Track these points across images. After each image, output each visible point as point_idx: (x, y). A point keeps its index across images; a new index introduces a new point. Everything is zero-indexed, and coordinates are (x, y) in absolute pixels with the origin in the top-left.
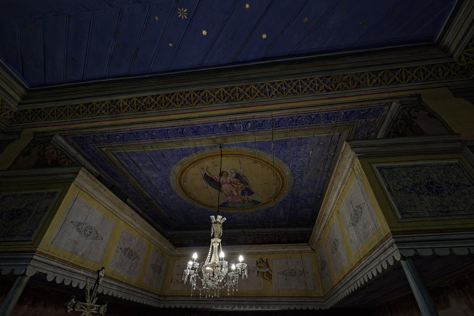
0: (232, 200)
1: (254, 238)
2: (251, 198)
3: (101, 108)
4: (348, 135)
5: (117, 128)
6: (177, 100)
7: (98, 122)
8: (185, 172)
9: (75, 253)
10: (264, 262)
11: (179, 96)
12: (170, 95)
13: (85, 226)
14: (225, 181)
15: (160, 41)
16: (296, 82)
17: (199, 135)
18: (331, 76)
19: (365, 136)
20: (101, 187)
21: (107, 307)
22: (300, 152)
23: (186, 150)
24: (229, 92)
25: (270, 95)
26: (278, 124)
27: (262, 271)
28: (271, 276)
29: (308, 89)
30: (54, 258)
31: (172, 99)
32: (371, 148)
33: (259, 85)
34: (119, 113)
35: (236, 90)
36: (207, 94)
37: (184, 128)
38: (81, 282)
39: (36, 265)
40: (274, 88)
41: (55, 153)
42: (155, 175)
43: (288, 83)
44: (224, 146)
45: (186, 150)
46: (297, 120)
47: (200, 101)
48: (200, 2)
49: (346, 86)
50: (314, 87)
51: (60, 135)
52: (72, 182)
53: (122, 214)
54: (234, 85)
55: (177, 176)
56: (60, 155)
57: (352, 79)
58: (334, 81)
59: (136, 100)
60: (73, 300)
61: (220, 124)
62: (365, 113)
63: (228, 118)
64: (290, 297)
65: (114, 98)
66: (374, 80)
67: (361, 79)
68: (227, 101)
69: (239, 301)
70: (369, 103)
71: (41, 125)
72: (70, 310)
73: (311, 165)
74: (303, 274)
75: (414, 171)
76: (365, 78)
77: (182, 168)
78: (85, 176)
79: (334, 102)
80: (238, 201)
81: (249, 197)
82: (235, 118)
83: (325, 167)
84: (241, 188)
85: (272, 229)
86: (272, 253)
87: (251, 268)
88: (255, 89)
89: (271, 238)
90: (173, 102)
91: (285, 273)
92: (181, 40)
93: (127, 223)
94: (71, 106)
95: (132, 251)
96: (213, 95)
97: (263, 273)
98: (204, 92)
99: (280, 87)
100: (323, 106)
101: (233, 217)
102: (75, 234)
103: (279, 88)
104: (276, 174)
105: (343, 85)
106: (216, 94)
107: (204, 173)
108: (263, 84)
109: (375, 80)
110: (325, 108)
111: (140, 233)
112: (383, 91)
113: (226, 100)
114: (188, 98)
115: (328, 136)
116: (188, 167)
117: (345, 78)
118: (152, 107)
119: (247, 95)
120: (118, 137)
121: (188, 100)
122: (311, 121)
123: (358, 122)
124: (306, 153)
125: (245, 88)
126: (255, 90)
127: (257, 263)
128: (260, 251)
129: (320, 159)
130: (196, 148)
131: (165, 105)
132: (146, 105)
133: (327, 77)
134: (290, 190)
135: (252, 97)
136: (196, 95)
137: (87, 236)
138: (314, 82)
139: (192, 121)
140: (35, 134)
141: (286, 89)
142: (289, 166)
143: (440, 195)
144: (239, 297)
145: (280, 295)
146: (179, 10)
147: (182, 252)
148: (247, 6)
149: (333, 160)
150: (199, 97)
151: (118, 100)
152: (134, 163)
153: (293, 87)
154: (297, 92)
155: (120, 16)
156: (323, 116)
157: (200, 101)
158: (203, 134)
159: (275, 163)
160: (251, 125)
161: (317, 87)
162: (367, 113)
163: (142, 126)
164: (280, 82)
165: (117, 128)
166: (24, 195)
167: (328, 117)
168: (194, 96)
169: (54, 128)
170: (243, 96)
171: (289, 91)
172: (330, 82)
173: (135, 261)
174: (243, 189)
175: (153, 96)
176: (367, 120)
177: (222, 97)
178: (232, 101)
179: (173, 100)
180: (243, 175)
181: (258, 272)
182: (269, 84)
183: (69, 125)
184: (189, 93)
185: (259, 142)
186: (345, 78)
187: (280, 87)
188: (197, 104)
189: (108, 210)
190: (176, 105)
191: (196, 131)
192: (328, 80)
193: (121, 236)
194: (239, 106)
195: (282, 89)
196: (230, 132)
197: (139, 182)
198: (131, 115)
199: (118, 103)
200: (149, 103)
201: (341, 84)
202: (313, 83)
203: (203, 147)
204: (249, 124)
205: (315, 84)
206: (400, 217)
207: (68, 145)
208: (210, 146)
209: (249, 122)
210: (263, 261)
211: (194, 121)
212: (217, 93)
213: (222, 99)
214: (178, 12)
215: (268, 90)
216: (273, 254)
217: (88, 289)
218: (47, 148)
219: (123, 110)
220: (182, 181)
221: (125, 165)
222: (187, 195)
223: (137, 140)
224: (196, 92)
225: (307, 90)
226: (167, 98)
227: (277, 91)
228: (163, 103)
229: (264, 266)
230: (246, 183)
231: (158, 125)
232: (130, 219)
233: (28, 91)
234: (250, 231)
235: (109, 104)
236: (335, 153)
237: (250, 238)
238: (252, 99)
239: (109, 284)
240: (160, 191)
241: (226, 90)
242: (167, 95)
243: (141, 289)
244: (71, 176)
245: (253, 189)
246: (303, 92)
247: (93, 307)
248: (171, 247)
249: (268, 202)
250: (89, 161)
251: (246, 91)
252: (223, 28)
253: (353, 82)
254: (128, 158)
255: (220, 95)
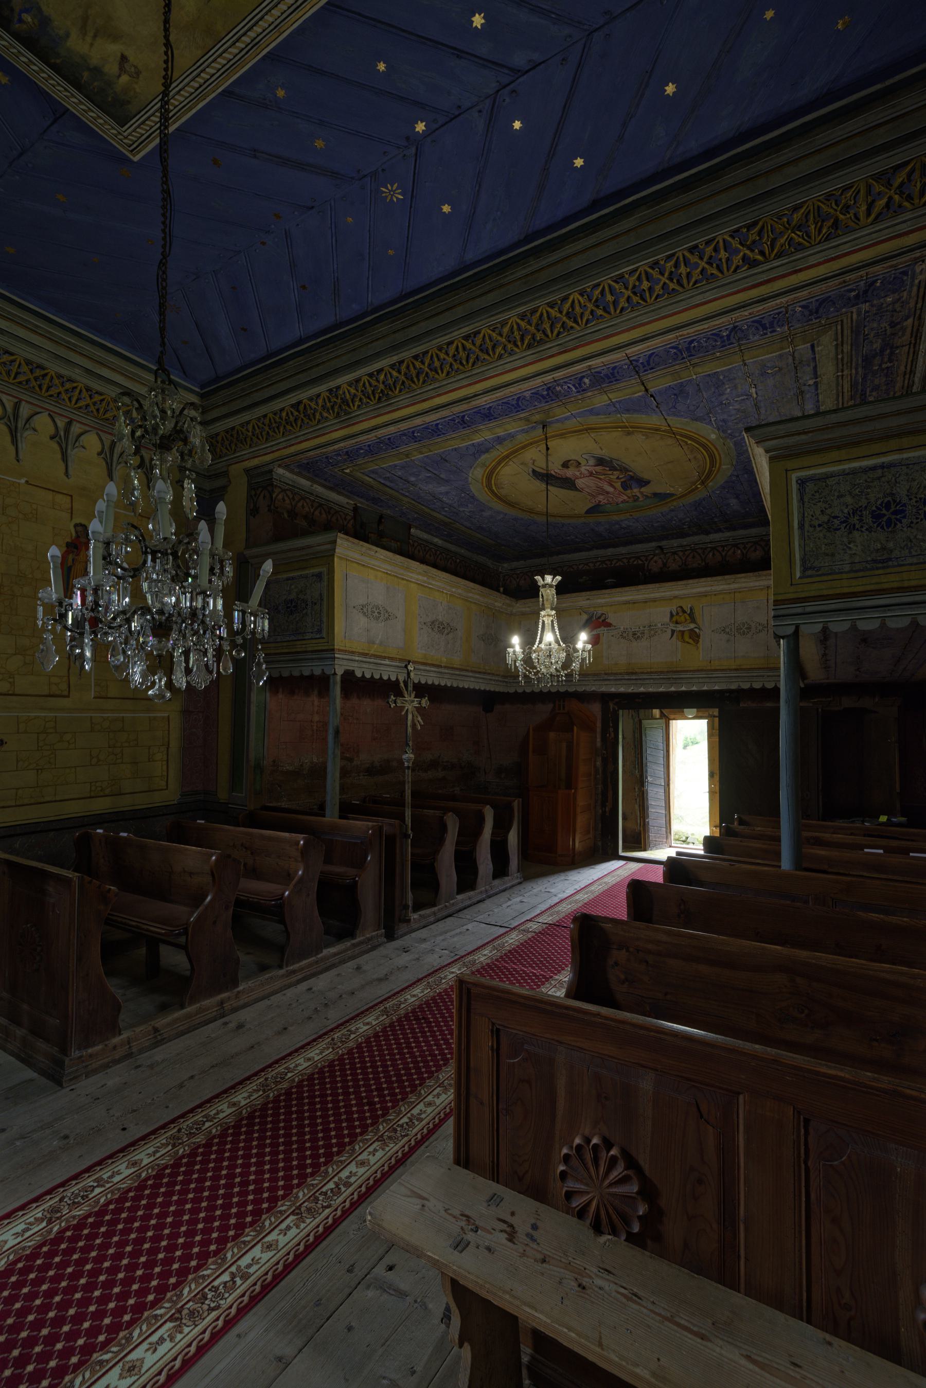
0: (608, 500)
1: (684, 558)
2: (646, 490)
3: (320, 408)
4: (836, 340)
5: (356, 440)
6: (435, 365)
7: (324, 434)
8: (494, 475)
9: (371, 642)
10: (686, 612)
11: (437, 355)
12: (421, 355)
13: (370, 607)
14: (578, 474)
15: (369, 253)
16: (673, 262)
17: (495, 418)
18: (760, 220)
19: (886, 330)
20: (370, 549)
21: (429, 699)
22: (725, 397)
23: (479, 444)
24: (529, 323)
25: (615, 311)
26: (649, 364)
27: (682, 629)
28: (698, 636)
29: (703, 271)
30: (353, 653)
31: (426, 365)
32: (796, 437)
33: (589, 290)
34: (350, 413)
35: (542, 315)
36: (487, 338)
37: (464, 416)
38: (390, 673)
39: (341, 663)
40: (623, 290)
41: (286, 498)
42: (443, 489)
43: (653, 269)
44: (551, 423)
45: (482, 444)
46: (688, 349)
47: (477, 358)
48: (418, 161)
49: (801, 240)
50: (718, 262)
51: (280, 466)
52: (333, 555)
53: (411, 575)
54: (537, 303)
55: (482, 483)
56: (293, 498)
57: (816, 214)
58: (768, 232)
59: (368, 381)
60: (392, 697)
61: (528, 394)
62: (861, 293)
63: (538, 381)
64: (730, 670)
65: (332, 384)
66: (881, 202)
67: (841, 209)
68: (529, 346)
69: (636, 679)
70: (863, 273)
71: (247, 455)
72: (393, 705)
73: (766, 411)
74: (766, 629)
75: (868, 480)
76: (852, 202)
77: (485, 471)
78: (346, 544)
79: (768, 292)
80: (620, 500)
81: (643, 489)
82: (553, 378)
83: (806, 407)
84: (618, 478)
85: (728, 534)
86: (705, 595)
87: (659, 625)
88: (582, 301)
89: (724, 554)
90: (431, 370)
91: (727, 630)
92: (408, 238)
93: (422, 585)
94: (275, 414)
95: (442, 623)
96: (499, 338)
97: (683, 632)
98: (482, 335)
99: (637, 284)
100: (742, 309)
101: (624, 525)
102: (363, 621)
103: (634, 287)
104: (686, 442)
105: (792, 238)
106: (505, 335)
107: (531, 470)
108: (598, 285)
109: (883, 202)
110: (746, 313)
111: (446, 594)
112: (904, 228)
113: (526, 342)
114: (454, 356)
115: (781, 356)
116: (495, 468)
117: (796, 217)
118: (398, 389)
119: (568, 321)
120: (362, 451)
121: (456, 361)
122: (724, 341)
123: (852, 313)
124: (742, 395)
125: (561, 304)
126: (583, 305)
127: (672, 615)
128: (677, 593)
129: (783, 398)
130: (498, 437)
131: (419, 380)
132: (386, 386)
133: (749, 227)
134: (734, 463)
135: (578, 324)
136: (468, 345)
137: (377, 619)
138: (716, 250)
139: (474, 403)
140: (247, 471)
141: (649, 284)
142: (710, 423)
143: (890, 529)
144: (636, 673)
145: (713, 668)
146: (384, 189)
147: (529, 607)
148: (517, 125)
149: (819, 391)
150: (473, 348)
151: (338, 388)
152: (401, 478)
153: (666, 275)
154: (677, 288)
155: (289, 241)
156: (749, 326)
157: (477, 358)
158: (502, 416)
159: (671, 425)
160: (590, 380)
161: (724, 261)
162: (866, 292)
163: (392, 429)
164: (635, 270)
165: (356, 440)
166: (288, 579)
167: (761, 325)
168: (464, 348)
169: (268, 458)
170: (559, 326)
171: (658, 289)
172: (758, 238)
173: (451, 636)
174: (622, 480)
175: (392, 366)
176: (875, 302)
177: (518, 337)
178: (538, 342)
179: (429, 365)
180: (611, 458)
181: (673, 632)
182: (610, 282)
183: (284, 448)
184: (455, 345)
185: (619, 402)
186: (796, 217)
187: (637, 284)
188: (473, 365)
189: (390, 574)
190: (436, 376)
191: (488, 415)
192: (753, 235)
193: (420, 607)
194: (555, 351)
195: (642, 287)
196: (552, 400)
197: (419, 503)
198: (368, 412)
199: (341, 392)
200: (390, 382)
201: (786, 237)
202: (713, 254)
203: (510, 434)
204: (587, 381)
205: (719, 253)
206: (798, 575)
207: (295, 477)
208: (523, 429)
209: (583, 377)
210: (684, 612)
211: (478, 402)
212: (506, 330)
213: (519, 343)
214: (384, 195)
215: (610, 299)
216: (706, 596)
217: (401, 679)
218: (274, 496)
219: (354, 406)
220: (494, 488)
221: (388, 484)
222: (513, 506)
223: (393, 448)
224: (466, 338)
225: (701, 277)
226: (418, 364)
227: (631, 295)
228: (414, 375)
229: (686, 620)
230: (624, 469)
231: (418, 421)
232: (425, 578)
233: (202, 396)
234: (675, 543)
235: (328, 397)
236: (816, 378)
237: (674, 560)
238: (579, 329)
239: (425, 670)
240: (461, 509)
241: (522, 320)
242: (416, 357)
243: (472, 671)
244: (328, 546)
245: (646, 476)
246: (691, 284)
247: (413, 701)
248: (508, 601)
249: (690, 492)
250: (331, 489)
251: (564, 312)
252: (480, 185)
253: (819, 224)
254: (388, 475)
255: (513, 333)
